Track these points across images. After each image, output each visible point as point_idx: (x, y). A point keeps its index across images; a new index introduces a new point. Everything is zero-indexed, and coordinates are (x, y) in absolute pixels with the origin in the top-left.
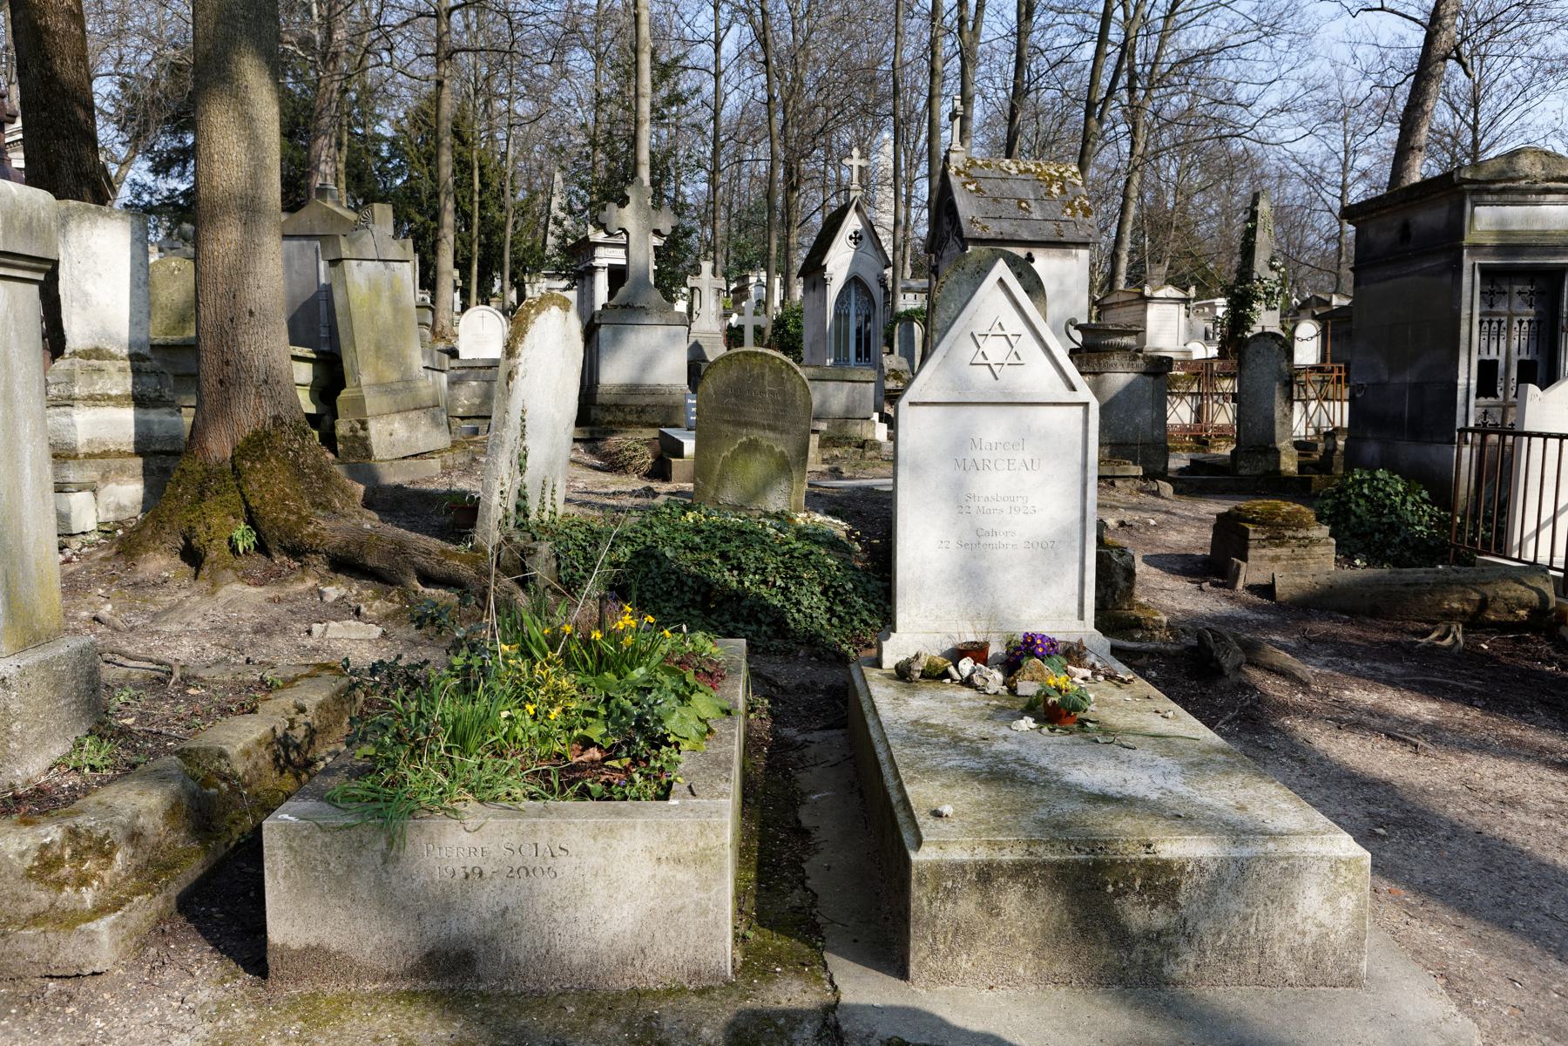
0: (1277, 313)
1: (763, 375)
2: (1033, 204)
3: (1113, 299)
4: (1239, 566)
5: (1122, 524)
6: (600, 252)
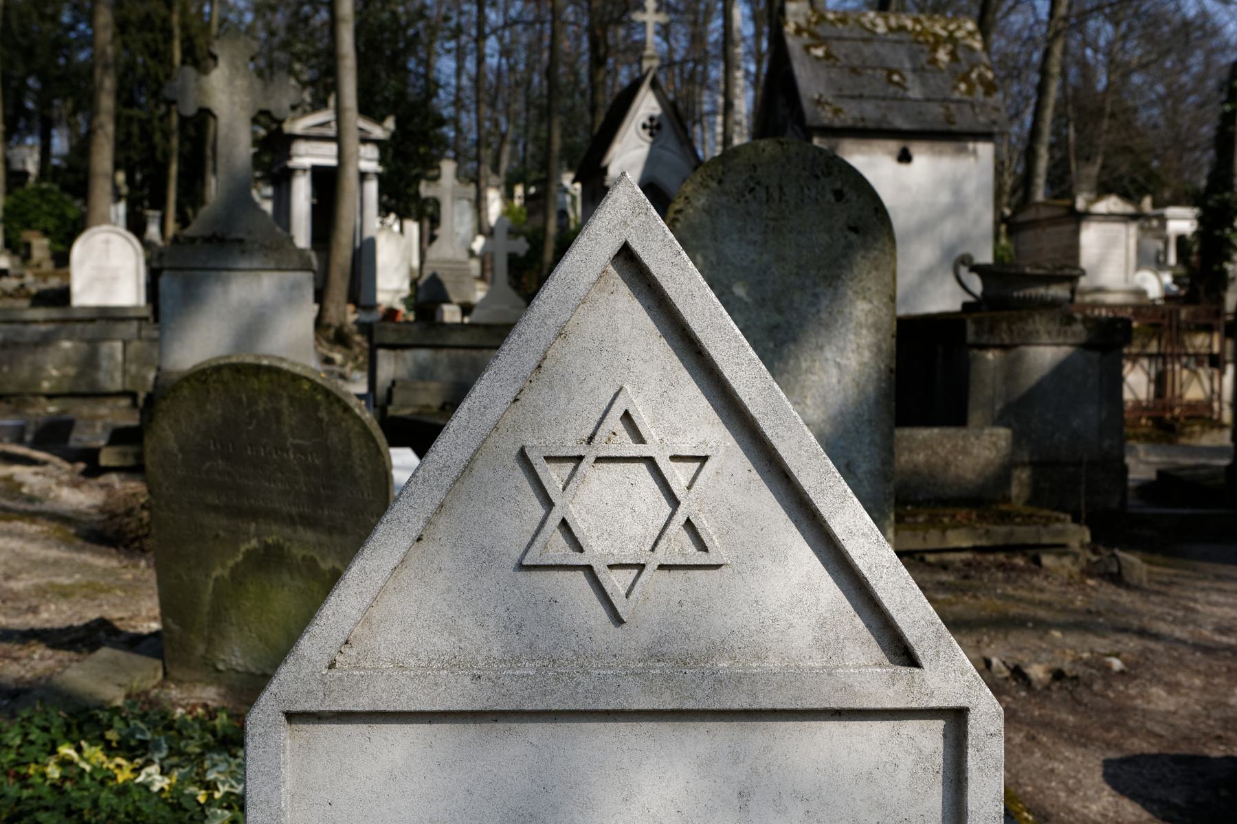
1: (278, 413)
2: (910, 76)
3: (1029, 215)
5: (1058, 675)
6: (300, 147)
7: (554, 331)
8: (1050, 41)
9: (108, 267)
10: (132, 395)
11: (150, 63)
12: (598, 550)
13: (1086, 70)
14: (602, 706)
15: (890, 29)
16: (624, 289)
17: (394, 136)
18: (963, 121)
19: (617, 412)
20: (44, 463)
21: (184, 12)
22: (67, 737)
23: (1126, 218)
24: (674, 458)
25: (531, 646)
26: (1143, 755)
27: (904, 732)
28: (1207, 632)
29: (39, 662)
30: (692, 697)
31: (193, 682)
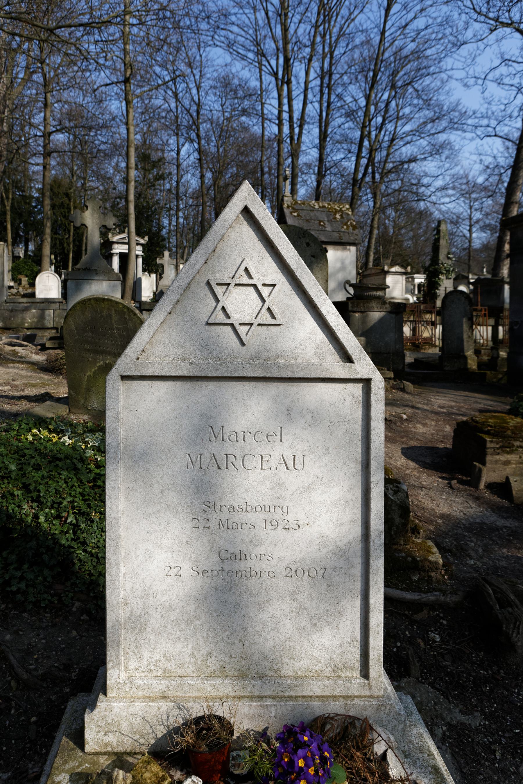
0: (451, 281)
1: (110, 316)
2: (327, 223)
3: (368, 272)
4: (480, 471)
6: (115, 246)
7: (220, 237)
8: (374, 216)
9: (48, 285)
10: (56, 329)
11: (63, 219)
12: (236, 318)
13: (386, 228)
14: (237, 375)
15: (320, 207)
16: (245, 223)
17: (147, 244)
18: (345, 239)
19: (243, 267)
20: (27, 346)
21: (75, 202)
22: (35, 427)
23: (401, 274)
24: (264, 285)
25: (211, 353)
26: (415, 446)
27: (347, 388)
28: (435, 407)
29: (25, 405)
30: (270, 372)
31: (79, 414)
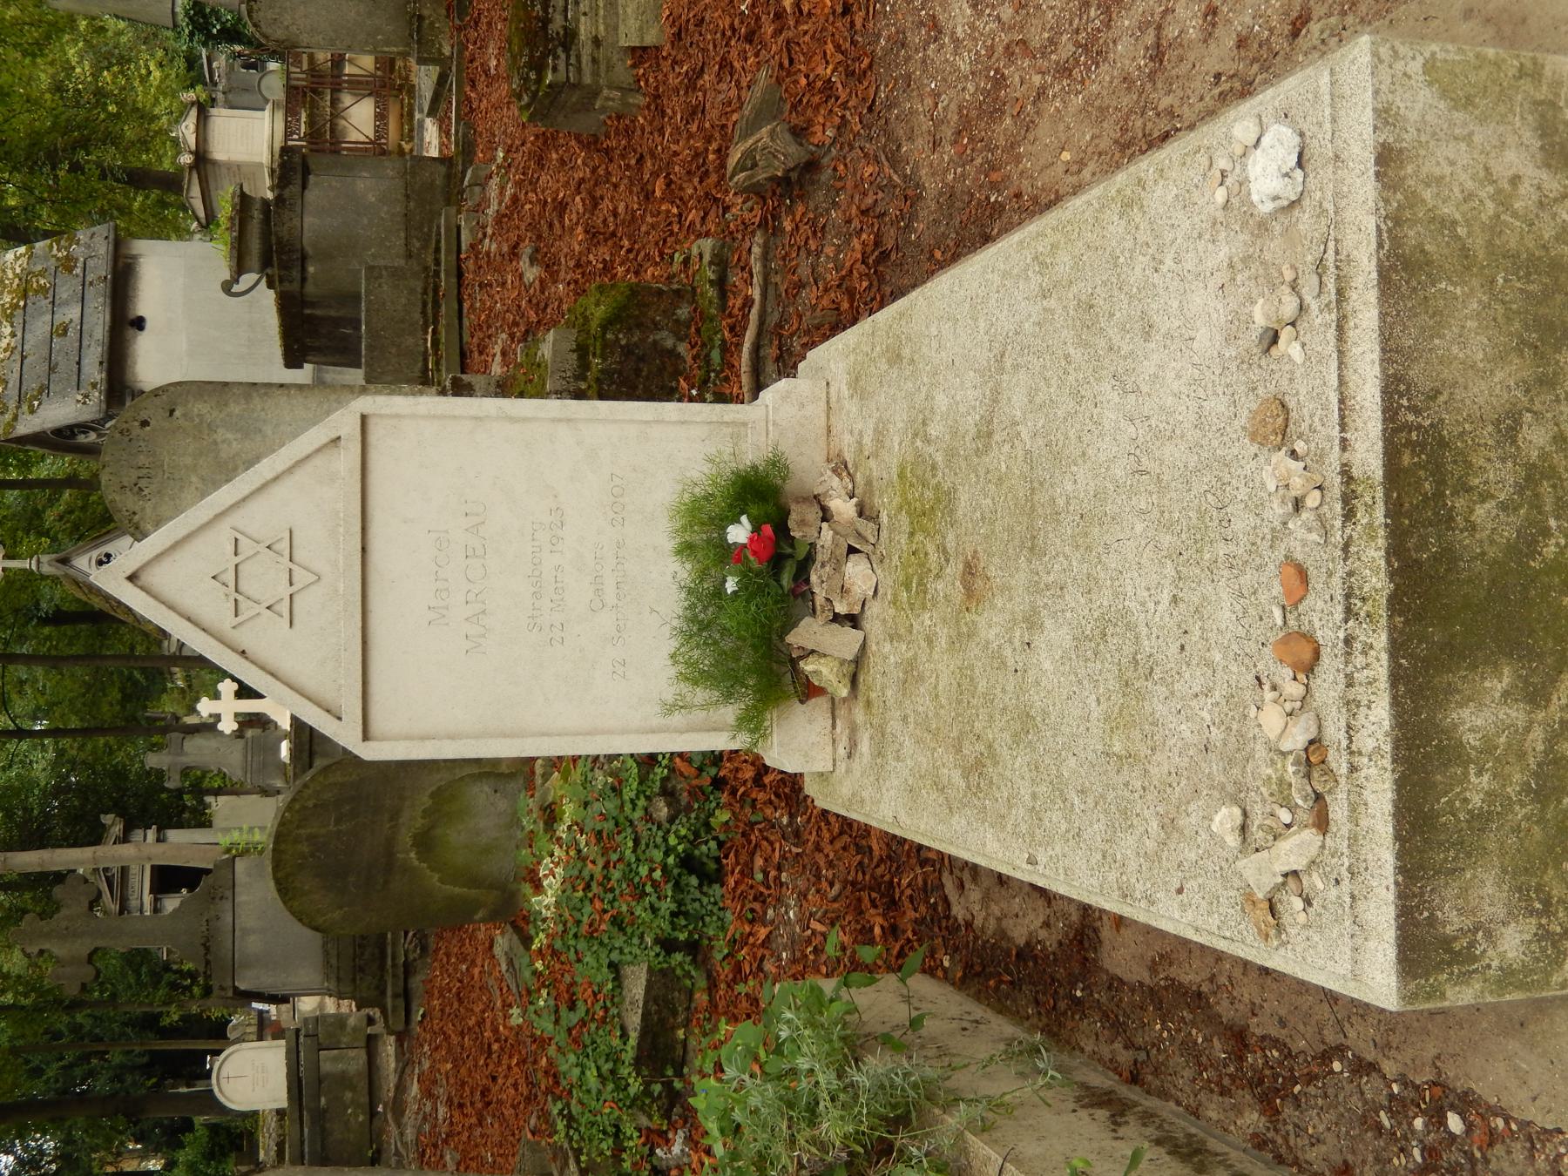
1: (311, 838)
